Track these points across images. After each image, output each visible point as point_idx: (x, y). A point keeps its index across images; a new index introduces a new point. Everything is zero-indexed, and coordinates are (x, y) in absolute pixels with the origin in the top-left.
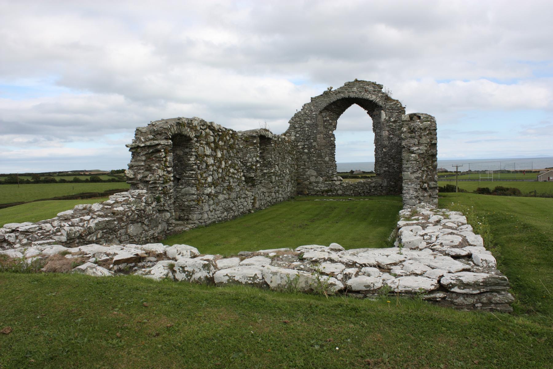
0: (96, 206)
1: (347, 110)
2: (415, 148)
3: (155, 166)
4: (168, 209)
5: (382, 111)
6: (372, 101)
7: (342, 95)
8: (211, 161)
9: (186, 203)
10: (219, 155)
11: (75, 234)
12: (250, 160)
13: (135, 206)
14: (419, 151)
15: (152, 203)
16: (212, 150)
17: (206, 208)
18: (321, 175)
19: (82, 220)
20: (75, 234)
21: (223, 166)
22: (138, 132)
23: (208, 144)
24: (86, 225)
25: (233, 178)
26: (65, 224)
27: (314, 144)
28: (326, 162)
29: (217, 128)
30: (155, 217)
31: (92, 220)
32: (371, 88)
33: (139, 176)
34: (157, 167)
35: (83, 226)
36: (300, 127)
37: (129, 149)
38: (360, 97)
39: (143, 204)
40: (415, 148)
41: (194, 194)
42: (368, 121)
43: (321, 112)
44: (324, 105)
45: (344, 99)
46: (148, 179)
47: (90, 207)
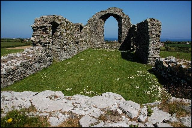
0: (18, 55)
1: (108, 18)
2: (154, 32)
3: (45, 35)
4: (50, 55)
8: (65, 34)
9: (56, 52)
10: (68, 32)
11: (10, 70)
12: (77, 35)
13: (37, 54)
14: (156, 34)
15: (44, 53)
17: (63, 54)
18: (99, 42)
19: (12, 62)
20: (10, 70)
21: (69, 37)
24: (15, 65)
25: (72, 42)
26: (4, 64)
27: (97, 30)
28: (101, 37)
30: (45, 59)
31: (17, 62)
33: (38, 40)
34: (46, 36)
35: (13, 65)
36: (91, 24)
38: (114, 13)
39: (41, 53)
40: (154, 32)
41: (59, 49)
42: (116, 22)
43: (99, 18)
44: (101, 16)
45: (108, 14)
46: (42, 42)
47: (16, 55)
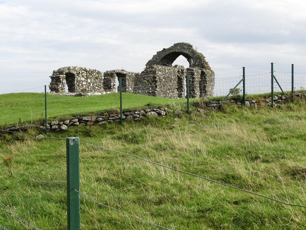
5: (192, 59)
6: (187, 54)
7: (172, 51)
14: (147, 79)
16: (85, 79)
22: (54, 72)
23: (83, 76)
29: (88, 70)
32: (186, 47)
37: (50, 78)
43: (161, 60)
44: (163, 56)
45: (173, 53)
